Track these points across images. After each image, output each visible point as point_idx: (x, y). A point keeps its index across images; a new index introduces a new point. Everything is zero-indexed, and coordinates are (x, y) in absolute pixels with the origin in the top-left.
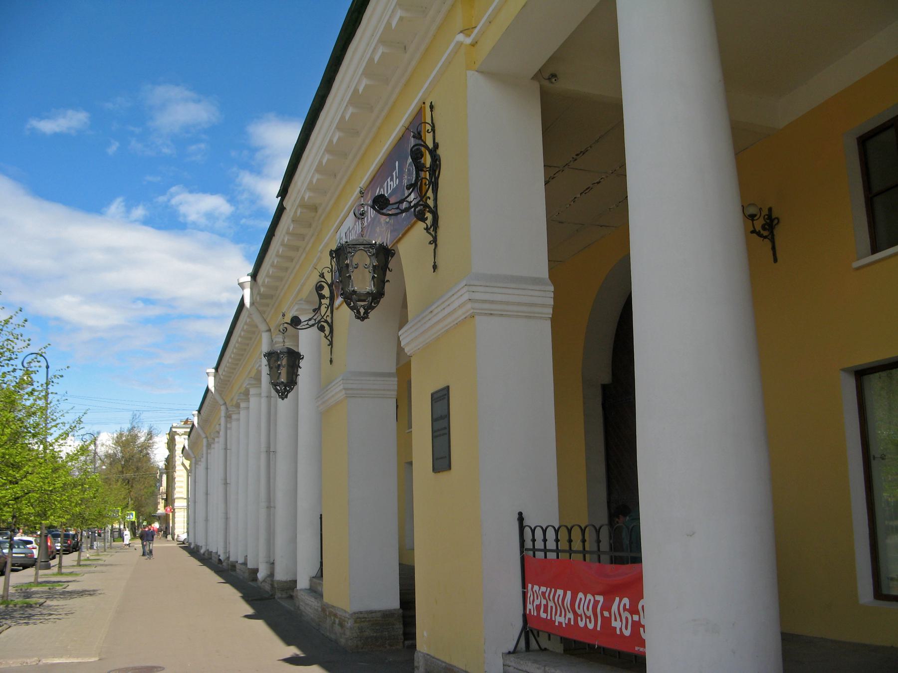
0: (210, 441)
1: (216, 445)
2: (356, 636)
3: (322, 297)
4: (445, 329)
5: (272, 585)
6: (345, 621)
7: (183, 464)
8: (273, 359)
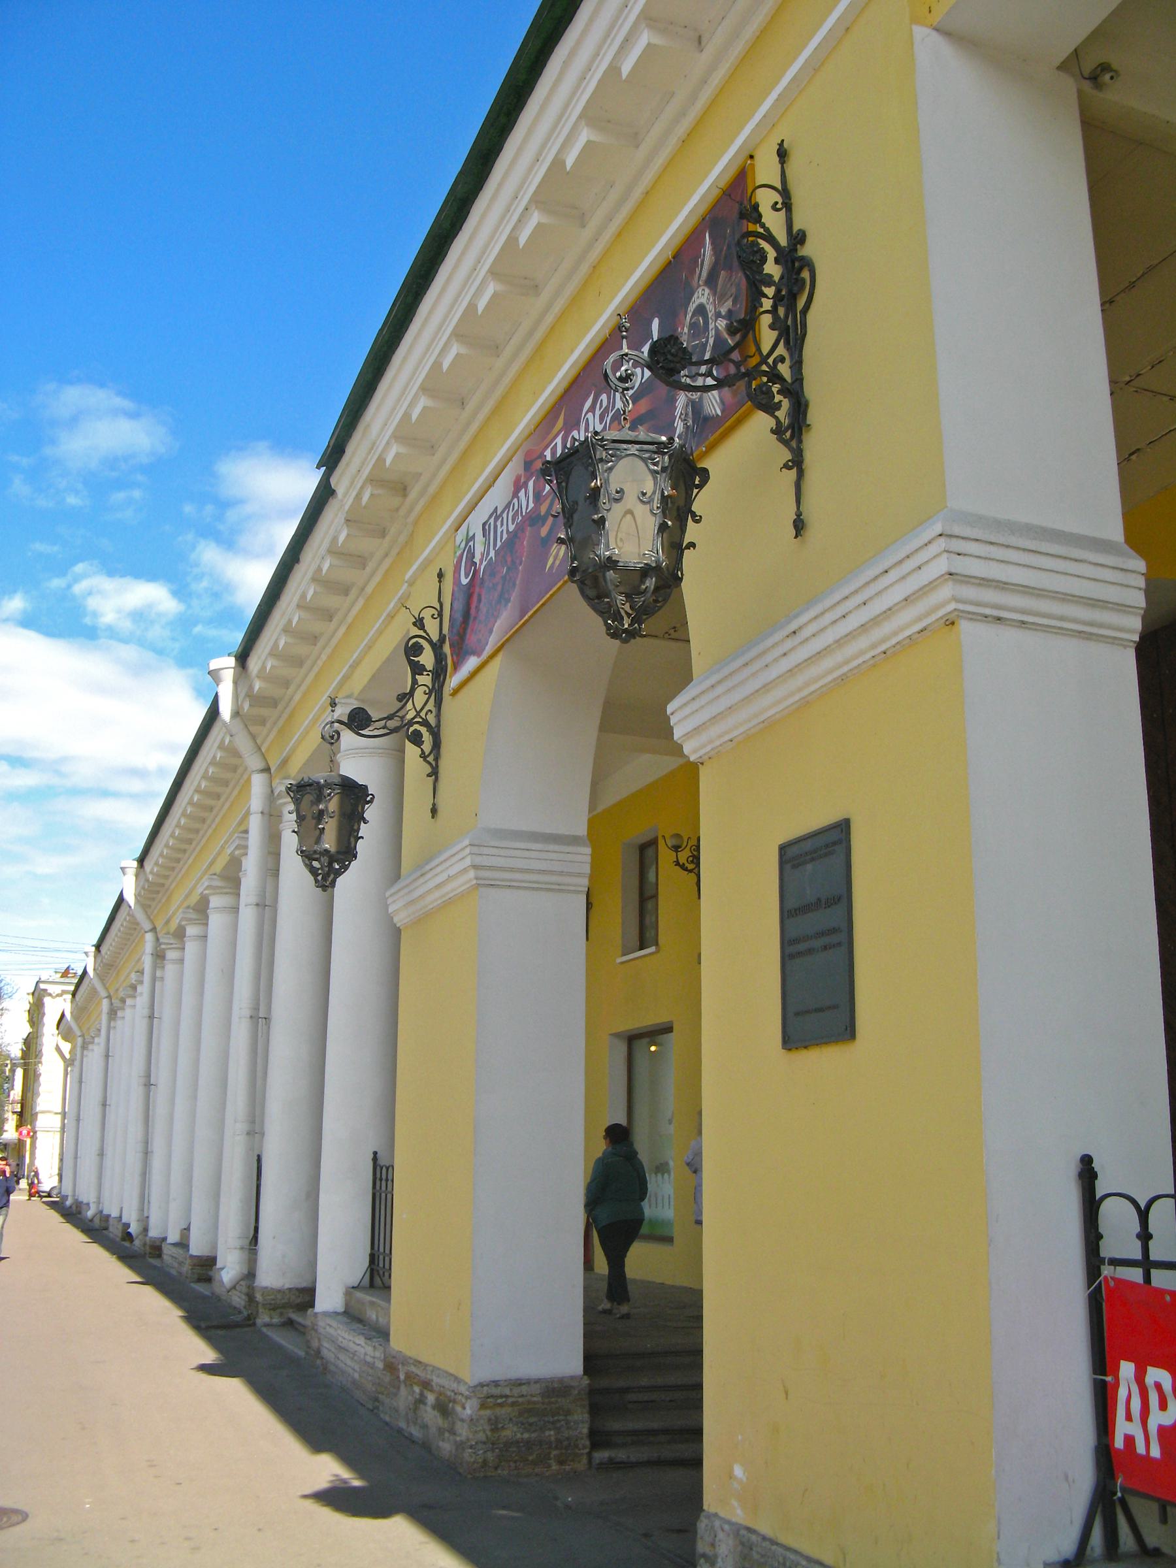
0: (115, 1005)
1: (128, 1012)
2: (484, 1439)
3: (417, 669)
4: (836, 674)
5: (251, 1297)
6: (454, 1401)
7: (58, 1049)
8: (308, 799)
